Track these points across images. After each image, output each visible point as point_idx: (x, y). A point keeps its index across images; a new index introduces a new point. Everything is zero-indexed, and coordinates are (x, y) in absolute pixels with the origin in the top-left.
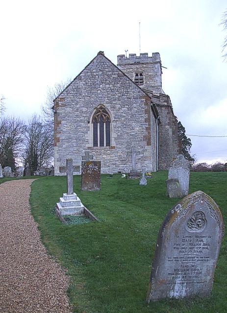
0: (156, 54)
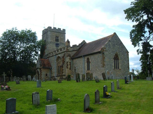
0: (64, 30)
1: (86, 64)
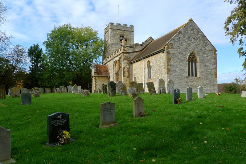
0: (132, 27)
1: (147, 70)
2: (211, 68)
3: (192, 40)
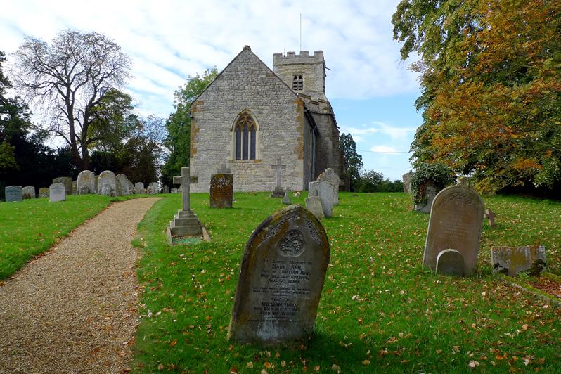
0: (319, 53)
2: (288, 139)
3: (246, 88)
